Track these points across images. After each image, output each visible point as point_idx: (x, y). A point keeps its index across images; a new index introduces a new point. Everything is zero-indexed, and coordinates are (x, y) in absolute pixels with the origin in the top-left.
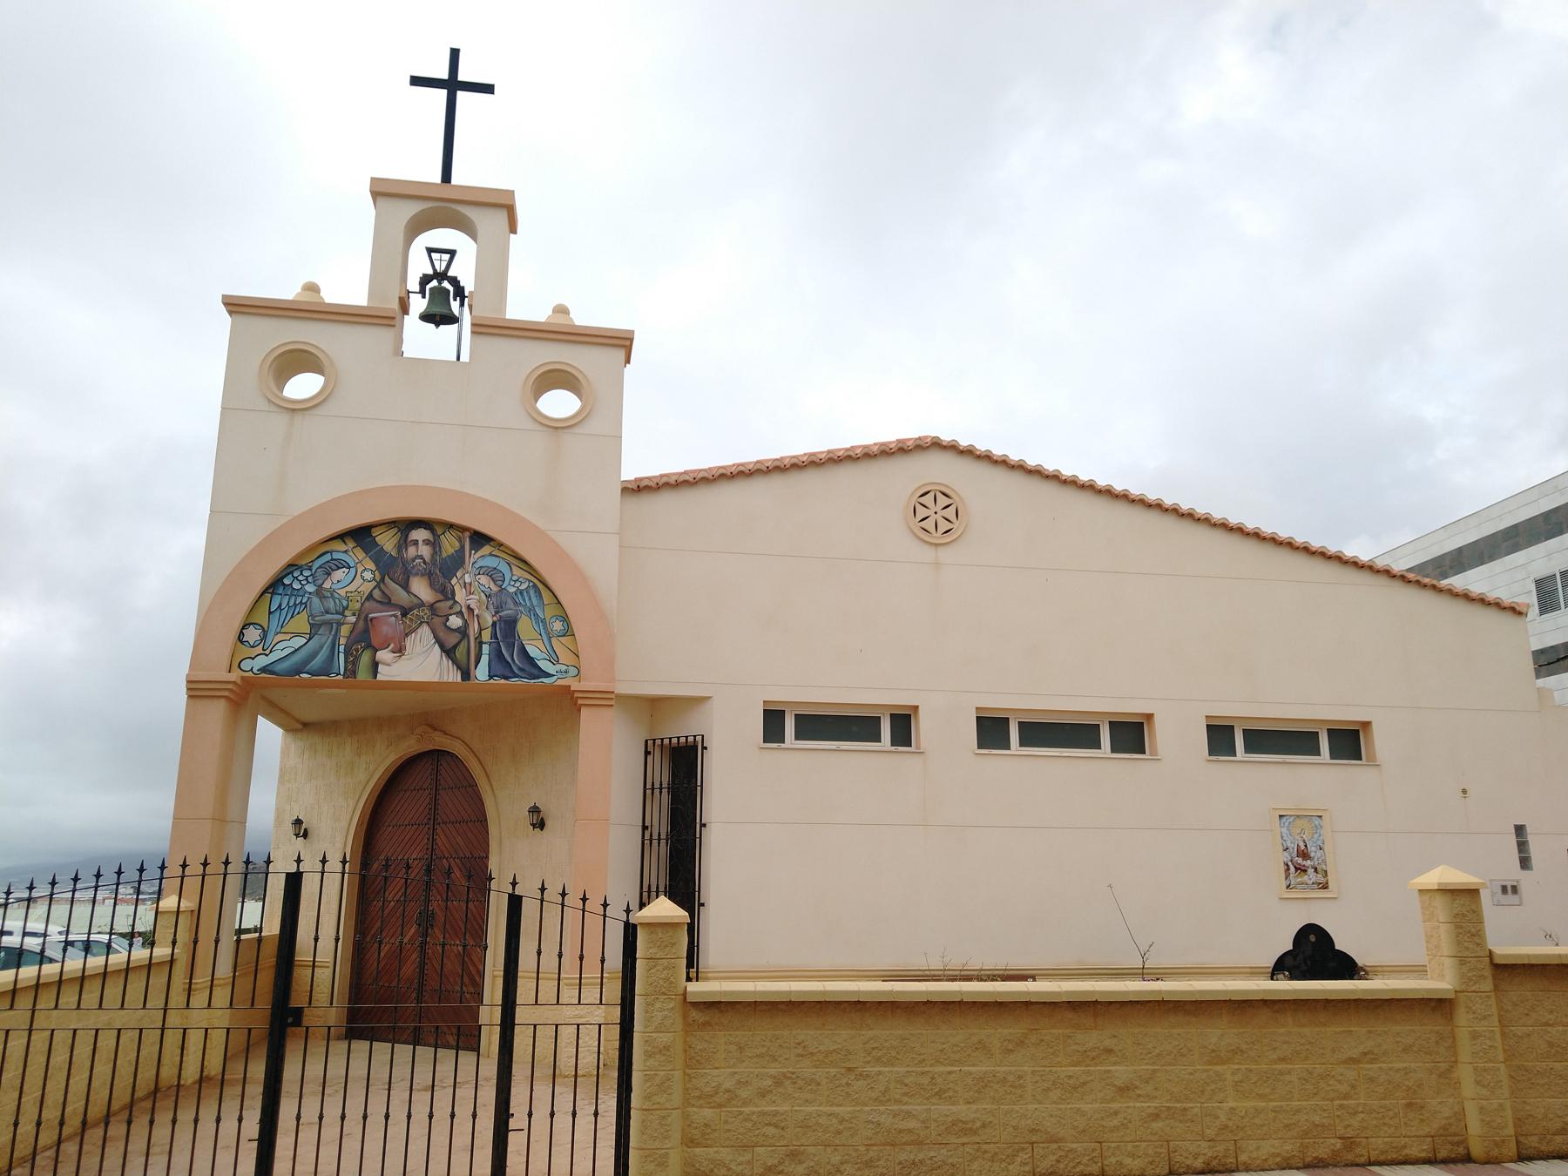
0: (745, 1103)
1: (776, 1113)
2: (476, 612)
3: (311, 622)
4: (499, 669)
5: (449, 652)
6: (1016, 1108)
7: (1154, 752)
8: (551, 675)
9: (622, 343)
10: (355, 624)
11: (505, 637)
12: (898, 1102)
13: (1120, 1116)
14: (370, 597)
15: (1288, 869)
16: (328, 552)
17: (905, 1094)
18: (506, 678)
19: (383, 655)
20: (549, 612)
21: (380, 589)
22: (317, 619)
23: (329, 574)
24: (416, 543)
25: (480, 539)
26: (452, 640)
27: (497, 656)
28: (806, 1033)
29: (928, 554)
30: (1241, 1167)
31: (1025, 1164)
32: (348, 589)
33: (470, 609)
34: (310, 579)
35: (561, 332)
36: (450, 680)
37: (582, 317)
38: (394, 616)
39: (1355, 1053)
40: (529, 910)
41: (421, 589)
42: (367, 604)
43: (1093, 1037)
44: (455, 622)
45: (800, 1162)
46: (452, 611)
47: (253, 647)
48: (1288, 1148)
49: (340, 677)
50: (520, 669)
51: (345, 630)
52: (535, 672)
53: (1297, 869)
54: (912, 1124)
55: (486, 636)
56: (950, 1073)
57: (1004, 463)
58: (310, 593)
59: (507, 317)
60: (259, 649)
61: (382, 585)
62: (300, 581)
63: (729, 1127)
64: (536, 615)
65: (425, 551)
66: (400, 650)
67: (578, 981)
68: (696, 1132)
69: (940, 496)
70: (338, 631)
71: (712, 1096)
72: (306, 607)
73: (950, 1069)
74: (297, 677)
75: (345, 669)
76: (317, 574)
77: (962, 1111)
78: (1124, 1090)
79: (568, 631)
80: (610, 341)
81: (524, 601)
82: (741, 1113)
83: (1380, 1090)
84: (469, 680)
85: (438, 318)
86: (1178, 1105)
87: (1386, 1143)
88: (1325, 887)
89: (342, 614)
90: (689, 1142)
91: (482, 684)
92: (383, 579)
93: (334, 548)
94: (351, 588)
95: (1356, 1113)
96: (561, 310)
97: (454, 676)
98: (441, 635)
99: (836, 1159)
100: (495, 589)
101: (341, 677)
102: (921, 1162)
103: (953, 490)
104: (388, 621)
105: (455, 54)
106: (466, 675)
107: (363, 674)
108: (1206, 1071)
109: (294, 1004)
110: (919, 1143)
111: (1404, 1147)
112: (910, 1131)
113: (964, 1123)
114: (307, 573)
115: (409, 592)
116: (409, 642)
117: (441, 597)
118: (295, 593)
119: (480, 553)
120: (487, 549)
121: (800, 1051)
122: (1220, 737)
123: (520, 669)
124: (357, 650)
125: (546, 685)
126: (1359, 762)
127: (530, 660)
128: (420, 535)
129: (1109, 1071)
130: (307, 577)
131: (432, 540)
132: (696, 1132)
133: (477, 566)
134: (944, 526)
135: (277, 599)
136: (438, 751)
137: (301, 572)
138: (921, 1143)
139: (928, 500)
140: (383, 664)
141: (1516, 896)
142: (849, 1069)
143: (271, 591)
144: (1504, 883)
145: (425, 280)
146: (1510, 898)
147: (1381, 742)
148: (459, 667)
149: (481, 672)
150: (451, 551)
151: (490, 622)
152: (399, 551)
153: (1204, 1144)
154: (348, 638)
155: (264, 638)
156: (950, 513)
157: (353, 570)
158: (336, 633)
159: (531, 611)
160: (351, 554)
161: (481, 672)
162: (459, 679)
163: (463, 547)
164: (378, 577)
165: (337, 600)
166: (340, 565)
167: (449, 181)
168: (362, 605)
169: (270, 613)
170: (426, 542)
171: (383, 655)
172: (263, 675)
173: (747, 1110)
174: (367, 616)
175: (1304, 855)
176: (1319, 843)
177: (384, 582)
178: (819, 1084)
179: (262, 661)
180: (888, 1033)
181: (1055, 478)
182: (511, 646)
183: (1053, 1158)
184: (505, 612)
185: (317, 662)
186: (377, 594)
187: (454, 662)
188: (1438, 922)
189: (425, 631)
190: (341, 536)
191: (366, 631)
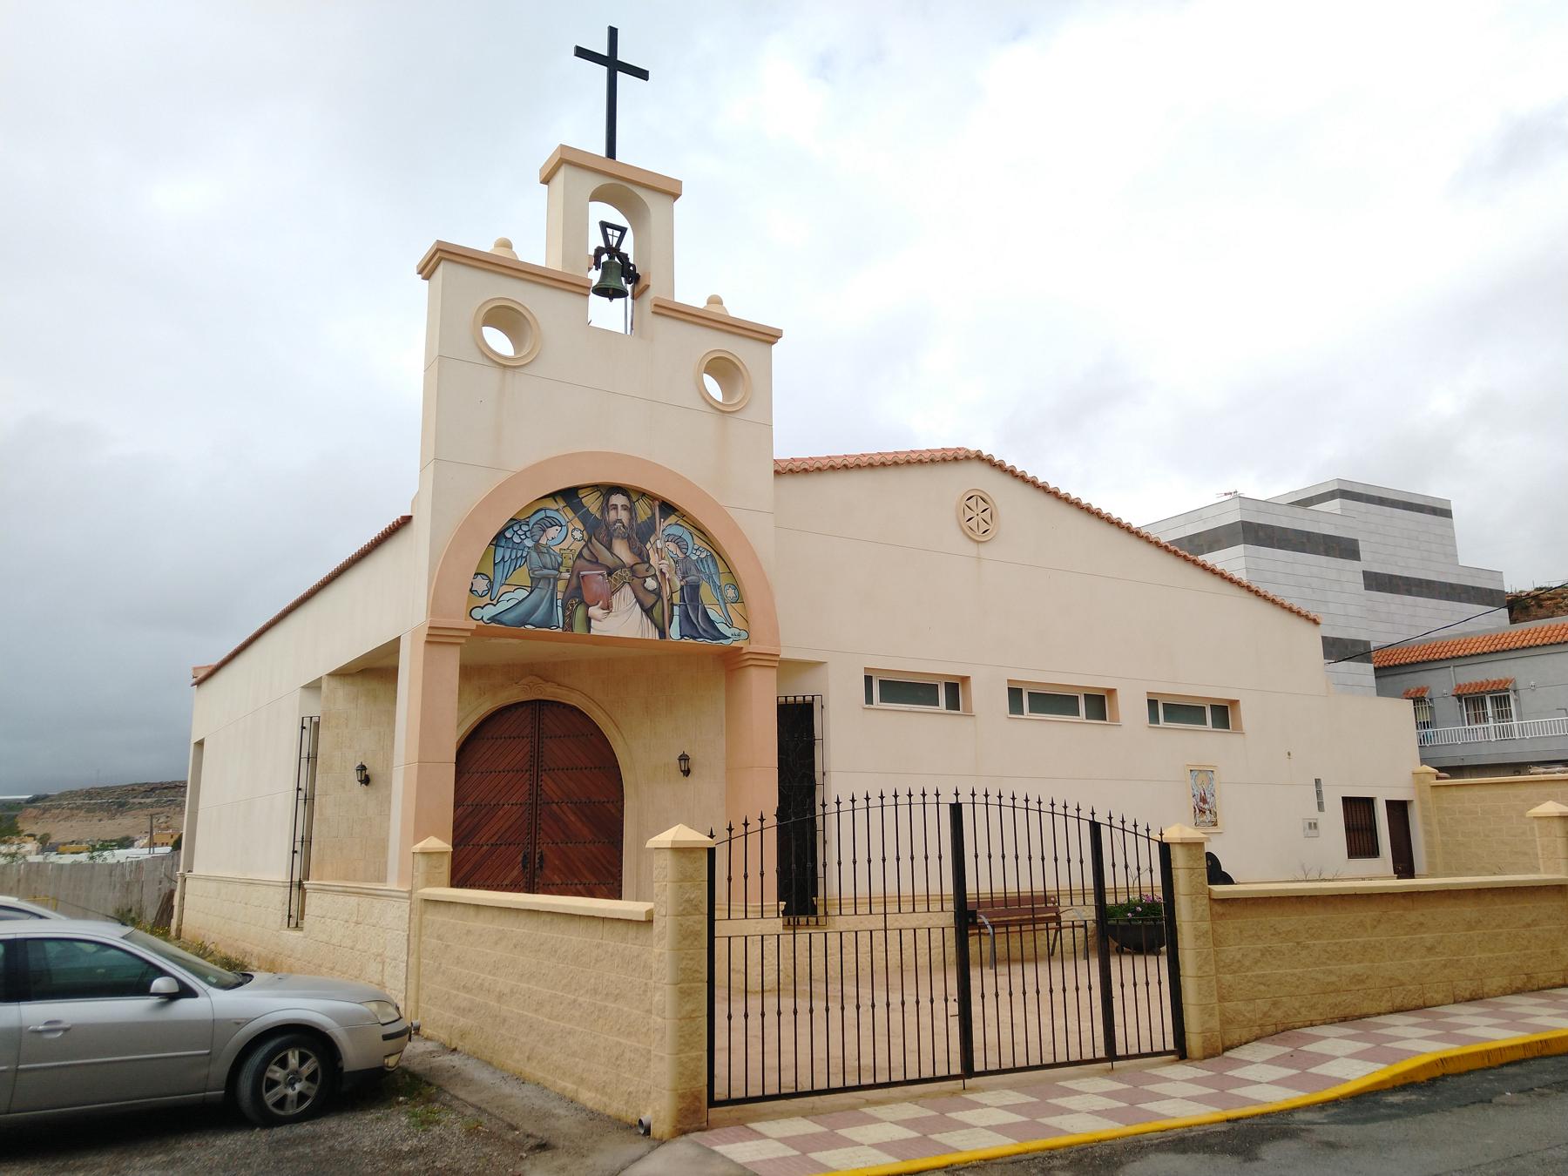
0: (1249, 969)
1: (1264, 976)
2: (667, 576)
3: (532, 575)
4: (687, 630)
5: (648, 611)
6: (1382, 964)
7: (1116, 719)
8: (727, 638)
9: (769, 337)
10: (569, 580)
11: (691, 600)
12: (1325, 963)
13: (1430, 966)
14: (580, 555)
15: (1195, 811)
16: (541, 510)
17: (1328, 959)
18: (694, 638)
19: (594, 611)
20: (723, 580)
21: (589, 549)
22: (536, 573)
23: (544, 531)
24: (615, 507)
25: (668, 508)
26: (650, 600)
27: (686, 617)
28: (1273, 919)
29: (971, 549)
30: (1485, 996)
31: (1389, 1001)
32: (561, 546)
33: (663, 573)
34: (528, 534)
35: (711, 320)
36: (650, 638)
37: (736, 309)
38: (603, 575)
39: (1529, 920)
40: (1105, 831)
41: (622, 551)
42: (578, 561)
43: (1414, 915)
44: (651, 584)
45: (1279, 1009)
46: (648, 574)
47: (481, 596)
48: (1505, 982)
49: (560, 630)
50: (704, 630)
51: (561, 585)
52: (716, 634)
53: (1200, 811)
54: (1334, 978)
55: (676, 598)
56: (1349, 943)
57: (1033, 483)
58: (529, 548)
59: (676, 301)
60: (487, 599)
61: (589, 545)
62: (520, 535)
63: (1240, 986)
64: (714, 582)
65: (624, 515)
66: (608, 608)
67: (760, 909)
68: (1224, 991)
69: (980, 501)
70: (555, 585)
71: (1230, 966)
72: (526, 560)
73: (1347, 940)
74: (523, 628)
75: (564, 623)
76: (534, 530)
77: (1356, 968)
78: (1430, 949)
79: (739, 599)
80: (756, 335)
81: (704, 568)
82: (1246, 976)
83: (1540, 943)
84: (665, 638)
85: (610, 292)
86: (1455, 958)
87: (1545, 976)
88: (1215, 825)
89: (558, 570)
90: (1222, 999)
91: (676, 643)
92: (590, 539)
93: (548, 506)
94: (564, 545)
95: (1530, 958)
96: (715, 300)
97: (653, 634)
98: (641, 595)
99: (1297, 1005)
100: (681, 556)
101: (560, 630)
102: (1340, 1003)
103: (991, 499)
104: (596, 580)
105: (613, 32)
106: (663, 634)
107: (579, 629)
108: (1466, 935)
109: (969, 908)
110: (1337, 991)
111: (1553, 977)
112: (1333, 983)
113: (1359, 976)
114: (525, 528)
115: (612, 553)
116: (615, 599)
117: (639, 561)
118: (516, 546)
119: (667, 522)
120: (673, 519)
121: (1272, 932)
122: (1099, 704)
123: (704, 630)
124: (572, 605)
125: (725, 646)
126: (1227, 730)
127: (711, 623)
128: (618, 500)
129: (1422, 938)
130: (526, 532)
131: (628, 505)
132: (1224, 991)
133: (666, 533)
134: (984, 527)
135: (500, 551)
136: (540, 701)
137: (520, 526)
138: (1339, 991)
139: (972, 503)
140: (596, 620)
141: (1316, 831)
142: (1298, 943)
143: (494, 543)
144: (1312, 821)
145: (599, 252)
146: (1313, 832)
147: (1247, 714)
148: (656, 626)
149: (674, 632)
150: (645, 518)
151: (679, 587)
152: (602, 513)
153: (1469, 982)
154: (565, 593)
155: (491, 588)
156: (986, 515)
157: (564, 529)
158: (554, 588)
159: (710, 577)
160: (562, 513)
161: (674, 632)
162: (658, 638)
163: (654, 514)
164: (586, 538)
165: (553, 557)
166: (553, 523)
167: (614, 158)
168: (574, 562)
169: (495, 564)
170: (624, 507)
171: (594, 611)
172: (493, 624)
173: (1249, 974)
174: (579, 573)
175: (1204, 800)
176: (1212, 791)
177: (591, 542)
178: (1284, 955)
179: (490, 611)
180: (1315, 917)
181: (1055, 494)
182: (696, 609)
183: (1402, 996)
184: (690, 578)
185: (539, 615)
186: (586, 553)
187: (652, 621)
188: (1556, 837)
189: (627, 590)
190: (553, 495)
191: (579, 588)
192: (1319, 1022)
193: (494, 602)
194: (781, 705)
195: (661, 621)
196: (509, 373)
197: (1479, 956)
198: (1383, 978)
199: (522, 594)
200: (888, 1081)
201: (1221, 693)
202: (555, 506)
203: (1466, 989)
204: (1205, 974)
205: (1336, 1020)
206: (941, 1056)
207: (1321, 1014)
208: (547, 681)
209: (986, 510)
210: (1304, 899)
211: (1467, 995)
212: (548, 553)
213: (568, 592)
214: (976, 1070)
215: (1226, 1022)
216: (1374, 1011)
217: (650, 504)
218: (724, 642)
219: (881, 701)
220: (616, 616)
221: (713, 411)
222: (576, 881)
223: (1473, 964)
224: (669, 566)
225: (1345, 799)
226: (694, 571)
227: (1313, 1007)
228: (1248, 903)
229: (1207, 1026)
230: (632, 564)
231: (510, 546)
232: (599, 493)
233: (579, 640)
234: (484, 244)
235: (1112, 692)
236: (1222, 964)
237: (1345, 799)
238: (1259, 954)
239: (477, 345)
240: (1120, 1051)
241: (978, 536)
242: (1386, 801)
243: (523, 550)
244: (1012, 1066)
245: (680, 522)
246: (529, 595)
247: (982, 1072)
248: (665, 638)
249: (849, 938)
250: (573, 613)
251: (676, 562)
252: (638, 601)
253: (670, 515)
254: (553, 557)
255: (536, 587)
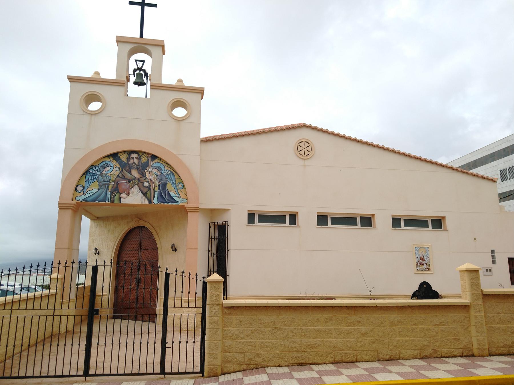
0: (242, 339)
1: (252, 342)
3: (99, 184)
4: (161, 200)
5: (144, 194)
7: (375, 227)
8: (177, 202)
9: (200, 92)
11: (163, 189)
12: (291, 338)
14: (118, 176)
16: (104, 161)
18: (163, 203)
19: (123, 195)
20: (177, 181)
22: (101, 183)
23: (104, 169)
24: (133, 158)
25: (154, 157)
26: (145, 190)
27: (160, 195)
29: (301, 162)
32: (111, 173)
33: (151, 180)
34: (98, 170)
35: (180, 88)
36: (145, 203)
37: (187, 83)
38: (126, 182)
39: (438, 323)
41: (135, 174)
42: (117, 178)
43: (354, 318)
44: (146, 184)
45: (260, 357)
48: (416, 352)
51: (110, 187)
52: (173, 201)
53: (420, 264)
54: (296, 345)
55: (157, 189)
56: (308, 329)
60: (82, 193)
61: (122, 172)
62: (95, 171)
64: (173, 182)
65: (136, 161)
66: (128, 194)
69: (305, 143)
70: (108, 187)
72: (97, 179)
75: (110, 200)
76: (100, 169)
77: (311, 341)
78: (363, 334)
79: (183, 188)
81: (169, 177)
82: (241, 342)
85: (139, 84)
88: (429, 270)
89: (109, 182)
90: (224, 351)
91: (155, 205)
92: (122, 170)
94: (112, 173)
95: (438, 341)
96: (180, 81)
97: (146, 202)
98: (142, 189)
99: (271, 356)
100: (159, 173)
104: (124, 184)
106: (150, 202)
107: (116, 201)
110: (298, 351)
111: (453, 352)
112: (295, 347)
114: (97, 168)
115: (131, 174)
116: (131, 191)
117: (142, 176)
118: (93, 175)
119: (154, 162)
120: (156, 161)
122: (396, 222)
124: (114, 194)
128: (134, 156)
129: (359, 328)
130: (97, 169)
131: (138, 157)
133: (153, 166)
134: (307, 153)
135: (87, 177)
139: (302, 144)
141: (491, 273)
143: (85, 174)
145: (135, 71)
146: (489, 273)
147: (448, 223)
148: (148, 199)
149: (155, 201)
150: (145, 161)
151: (158, 185)
154: (111, 190)
160: (112, 162)
161: (155, 201)
162: (148, 203)
163: (148, 160)
164: (121, 170)
165: (107, 177)
166: (108, 166)
167: (142, 37)
169: (85, 181)
170: (136, 158)
171: (123, 195)
173: (243, 341)
175: (423, 259)
179: (83, 197)
180: (288, 316)
182: (165, 192)
186: (120, 175)
189: (136, 187)
190: (108, 156)
191: (117, 187)
192: (284, 365)
193: (85, 194)
194: (219, 225)
195: (150, 197)
196: (93, 117)
197: (398, 339)
198: (329, 346)
199: (95, 191)
200: (131, 373)
201: (437, 214)
202: (109, 160)
203: (386, 355)
204: (213, 340)
205: (308, 364)
206: (74, 366)
207: (286, 361)
208: (140, 219)
209: (299, 146)
210: (282, 308)
211: (387, 358)
212: (106, 176)
213: (113, 189)
214: (166, 371)
215: (226, 361)
216: (321, 362)
217: (147, 157)
218: (176, 203)
219: (258, 223)
220: (131, 196)
221: (175, 121)
222: (149, 288)
223: (393, 343)
224: (154, 177)
225: (509, 259)
226: (164, 178)
227: (282, 358)
228: (246, 308)
229: (212, 363)
230: (139, 177)
231: (91, 175)
232: (126, 154)
233: (116, 205)
234: (89, 74)
235: (373, 215)
236: (227, 336)
237: (509, 259)
238: (250, 332)
239: (82, 109)
240: (167, 370)
241: (305, 157)
242: (508, 258)
243: (96, 176)
244: (138, 372)
245: (160, 161)
246: (98, 191)
247: (137, 374)
248: (151, 203)
249: (21, 319)
250: (114, 196)
251: (157, 176)
252: (141, 190)
253: (155, 159)
254: (107, 177)
255: (101, 188)
